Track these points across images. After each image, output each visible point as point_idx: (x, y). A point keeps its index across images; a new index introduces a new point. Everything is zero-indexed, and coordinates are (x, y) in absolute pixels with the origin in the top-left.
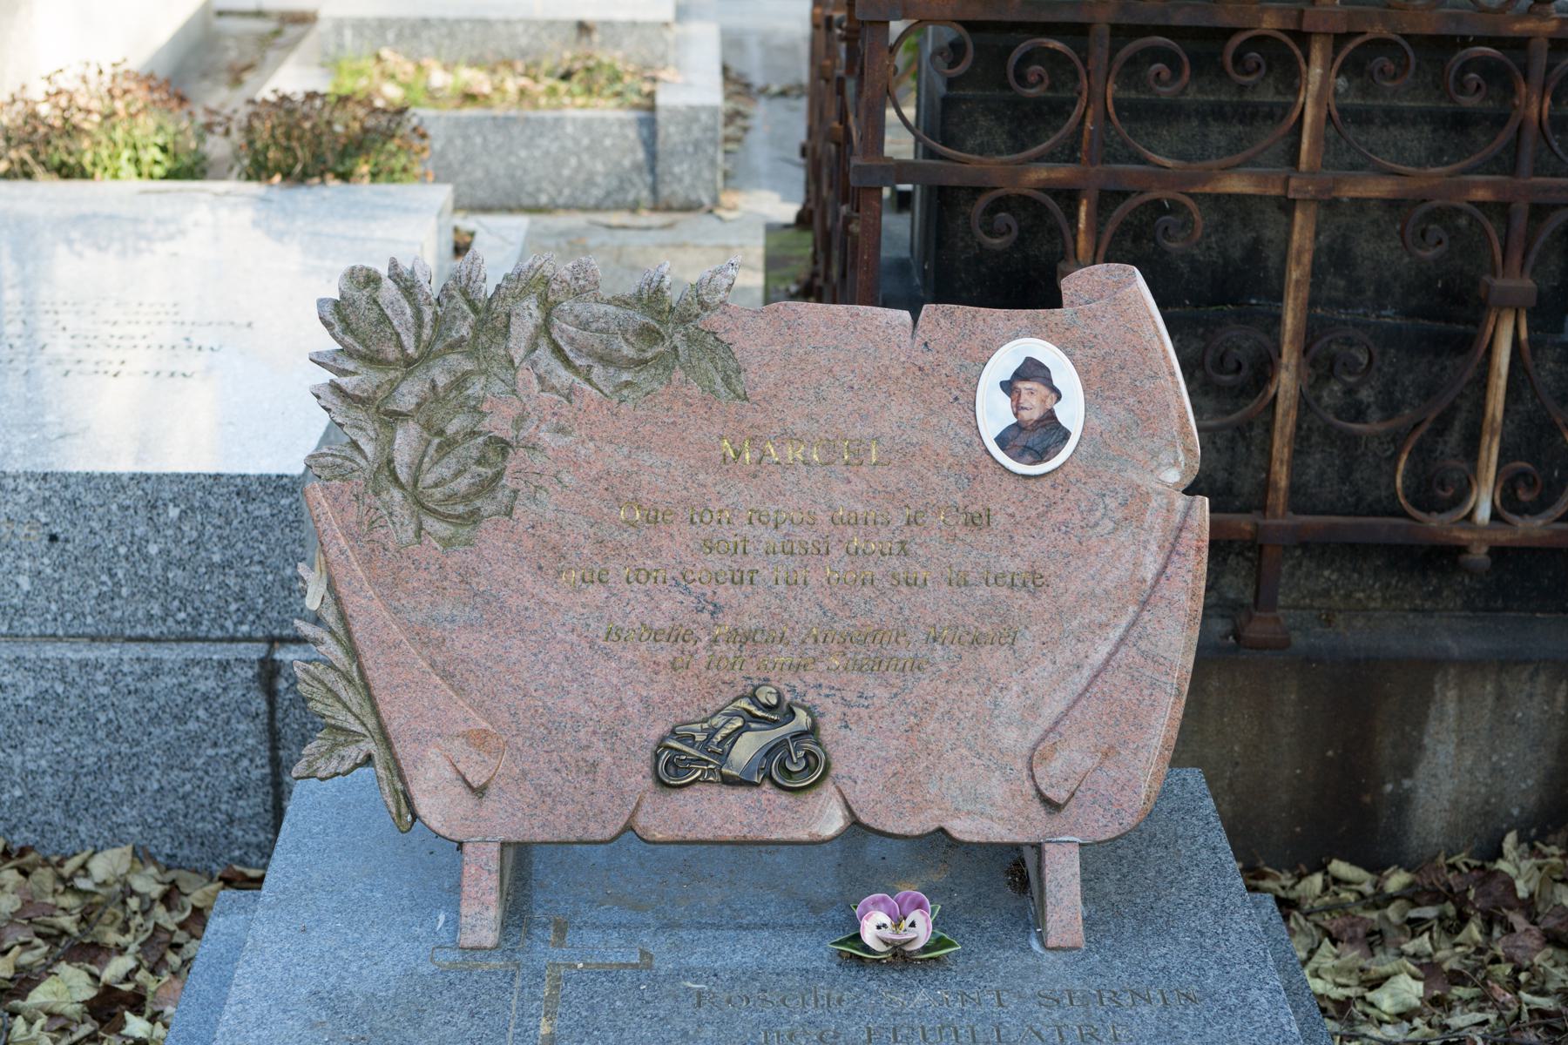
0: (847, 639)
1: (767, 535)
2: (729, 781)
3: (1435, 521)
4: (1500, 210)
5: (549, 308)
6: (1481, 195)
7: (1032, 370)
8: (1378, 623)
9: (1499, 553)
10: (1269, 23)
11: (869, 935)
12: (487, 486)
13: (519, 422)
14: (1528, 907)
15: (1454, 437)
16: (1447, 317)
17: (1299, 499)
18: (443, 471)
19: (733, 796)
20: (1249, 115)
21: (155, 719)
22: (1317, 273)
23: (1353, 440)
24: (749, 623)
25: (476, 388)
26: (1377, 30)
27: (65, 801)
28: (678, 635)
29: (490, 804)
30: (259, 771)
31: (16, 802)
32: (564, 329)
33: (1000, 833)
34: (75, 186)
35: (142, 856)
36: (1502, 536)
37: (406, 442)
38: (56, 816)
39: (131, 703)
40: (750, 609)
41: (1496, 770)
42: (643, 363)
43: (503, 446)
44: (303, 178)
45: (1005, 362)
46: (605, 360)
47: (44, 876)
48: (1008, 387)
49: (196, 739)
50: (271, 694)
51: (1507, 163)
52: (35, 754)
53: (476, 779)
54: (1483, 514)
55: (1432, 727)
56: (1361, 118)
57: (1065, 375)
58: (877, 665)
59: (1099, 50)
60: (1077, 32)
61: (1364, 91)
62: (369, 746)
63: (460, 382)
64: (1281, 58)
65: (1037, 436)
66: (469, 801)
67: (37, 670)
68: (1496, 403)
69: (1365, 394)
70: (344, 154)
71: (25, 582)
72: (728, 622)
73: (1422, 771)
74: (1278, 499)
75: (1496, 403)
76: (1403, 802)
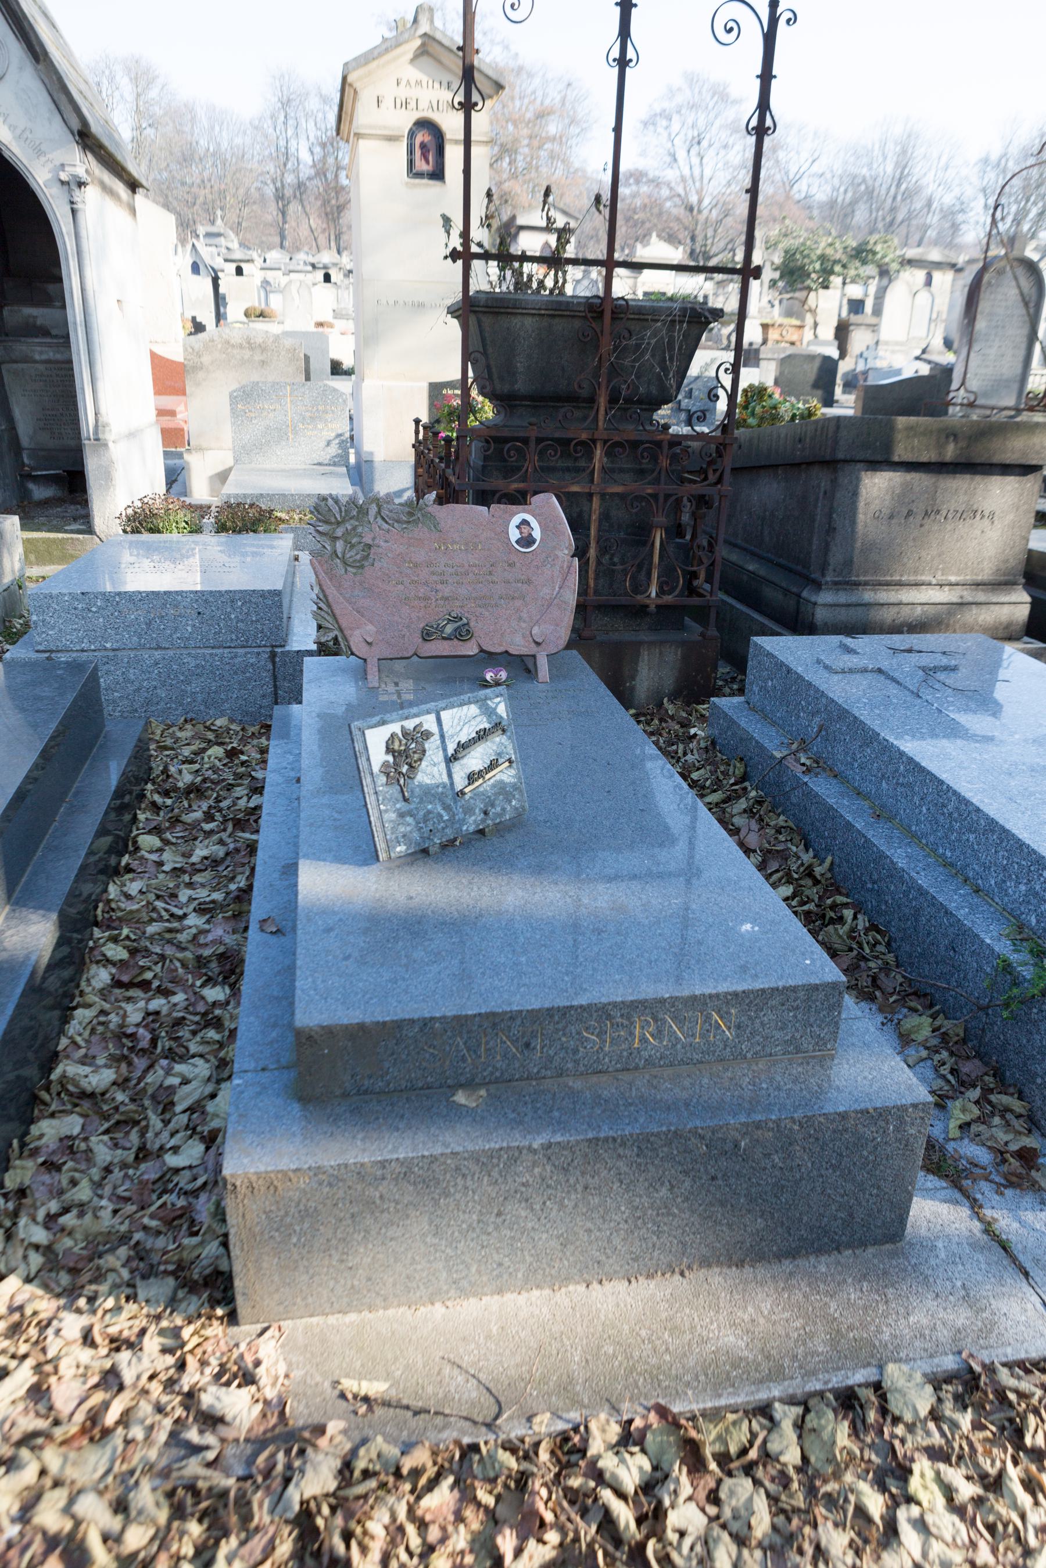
0: (475, 599)
1: (450, 570)
2: (444, 638)
3: (639, 597)
4: (655, 496)
5: (379, 507)
6: (649, 491)
7: (525, 522)
8: (622, 632)
9: (658, 607)
10: (584, 436)
11: (488, 678)
12: (366, 558)
13: (374, 539)
14: (672, 718)
15: (643, 573)
16: (640, 534)
17: (596, 592)
18: (352, 553)
19: (445, 643)
20: (578, 470)
21: (236, 673)
22: (600, 521)
23: (613, 571)
24: (446, 595)
25: (360, 530)
26: (617, 439)
27: (205, 702)
28: (426, 598)
29: (373, 648)
30: (270, 689)
31: (189, 703)
32: (385, 513)
33: (524, 651)
34: (157, 535)
35: (232, 720)
36: (659, 602)
37: (340, 545)
38: (202, 708)
39: (227, 667)
40: (446, 591)
41: (660, 678)
42: (409, 522)
43: (369, 546)
44: (240, 532)
45: (516, 520)
46: (398, 521)
47: (201, 727)
48: (518, 527)
49: (249, 679)
50: (274, 663)
51: (657, 481)
52: (195, 686)
53: (369, 640)
54: (653, 594)
55: (640, 664)
56: (613, 470)
57: (534, 523)
58: (485, 606)
59: (532, 444)
60: (525, 441)
61: (612, 462)
62: (336, 632)
63: (354, 528)
64: (587, 447)
65: (527, 541)
66: (367, 647)
67: (196, 657)
68: (656, 559)
69: (616, 560)
70: (253, 524)
71: (189, 629)
72: (440, 595)
73: (638, 679)
74: (591, 591)
75: (656, 559)
76: (632, 689)
